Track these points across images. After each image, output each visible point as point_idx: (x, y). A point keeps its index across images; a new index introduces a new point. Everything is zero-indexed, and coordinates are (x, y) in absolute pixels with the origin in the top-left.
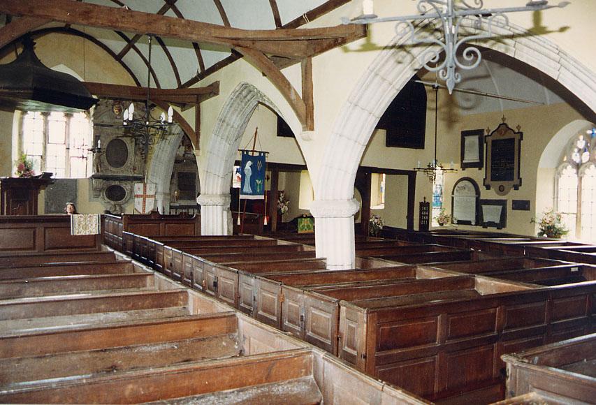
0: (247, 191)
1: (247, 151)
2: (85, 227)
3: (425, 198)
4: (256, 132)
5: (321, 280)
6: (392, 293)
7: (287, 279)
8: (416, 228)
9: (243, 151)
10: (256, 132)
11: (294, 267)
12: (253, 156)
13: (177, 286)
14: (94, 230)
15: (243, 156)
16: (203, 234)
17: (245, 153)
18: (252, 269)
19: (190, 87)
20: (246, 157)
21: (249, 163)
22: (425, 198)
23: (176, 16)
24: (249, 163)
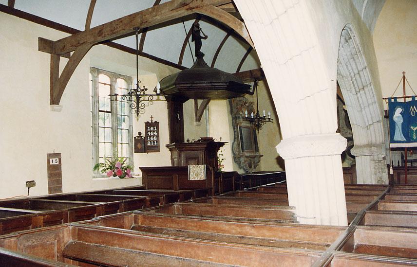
0: (400, 139)
1: (395, 99)
2: (197, 175)
3: (152, 117)
4: (404, 77)
5: (196, 226)
6: (158, 249)
7: (160, 220)
8: (400, 166)
9: (390, 99)
10: (404, 77)
11: (252, 214)
12: (405, 102)
13: (361, 236)
14: (202, 177)
15: (390, 103)
16: (358, 183)
17: (393, 100)
18: (208, 211)
19: (60, 74)
20: (393, 104)
21: (399, 110)
22: (152, 117)
23: (68, 35)
24: (399, 110)
